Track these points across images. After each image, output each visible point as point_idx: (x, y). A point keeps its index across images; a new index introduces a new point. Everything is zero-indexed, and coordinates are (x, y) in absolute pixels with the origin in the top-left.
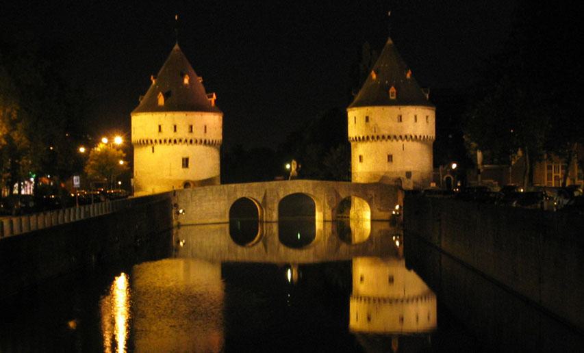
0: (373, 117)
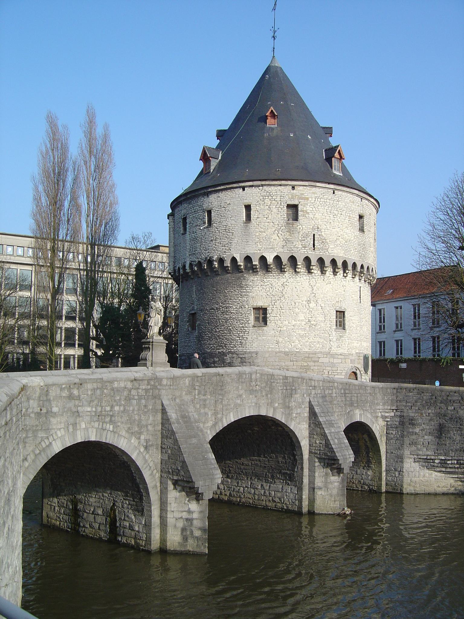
0: (308, 208)
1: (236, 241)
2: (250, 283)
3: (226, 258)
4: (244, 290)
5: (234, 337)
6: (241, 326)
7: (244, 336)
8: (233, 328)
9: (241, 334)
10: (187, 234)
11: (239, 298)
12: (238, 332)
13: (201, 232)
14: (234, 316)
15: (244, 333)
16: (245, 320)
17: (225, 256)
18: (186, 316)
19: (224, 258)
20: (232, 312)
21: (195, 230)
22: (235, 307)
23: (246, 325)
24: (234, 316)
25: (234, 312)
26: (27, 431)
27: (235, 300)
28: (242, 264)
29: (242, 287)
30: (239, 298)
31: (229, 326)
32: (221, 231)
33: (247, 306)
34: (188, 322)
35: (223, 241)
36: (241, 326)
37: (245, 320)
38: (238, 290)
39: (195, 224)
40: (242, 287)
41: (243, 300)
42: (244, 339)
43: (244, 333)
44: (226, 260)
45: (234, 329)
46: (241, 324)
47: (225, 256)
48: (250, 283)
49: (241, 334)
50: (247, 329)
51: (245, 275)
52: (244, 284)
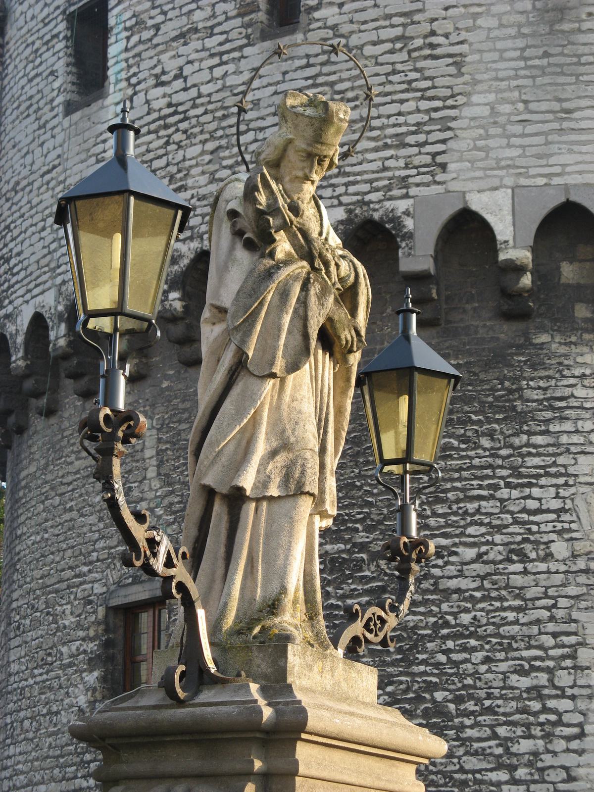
1: (486, 111)
2: (579, 392)
3: (409, 223)
4: (539, 440)
5: (471, 763)
6: (525, 682)
7: (548, 760)
8: (458, 700)
9: (525, 746)
10: (110, 100)
11: (504, 493)
12: (502, 731)
13: (218, 72)
14: (466, 618)
15: (548, 737)
16: (549, 641)
17: (402, 205)
18: (79, 626)
19: (396, 221)
20: (453, 584)
21: (171, 65)
22: (470, 553)
23: (564, 679)
24: (466, 618)
25: (463, 584)
26: (167, 475)
27: (471, 507)
28: (524, 256)
29: (522, 418)
30: (504, 493)
31: (431, 687)
32: (369, 50)
33: (560, 549)
34: (92, 664)
35: (383, 110)
36: (525, 682)
37: (549, 641)
38: (491, 435)
39: (170, 29)
40: (522, 418)
41: (532, 504)
42: (552, 776)
43: (548, 737)
44: (410, 236)
45: (470, 706)
46: (521, 672)
47: (402, 205)
48: (579, 392)
49: (525, 746)
50: (564, 705)
51: (544, 338)
52: (537, 395)
